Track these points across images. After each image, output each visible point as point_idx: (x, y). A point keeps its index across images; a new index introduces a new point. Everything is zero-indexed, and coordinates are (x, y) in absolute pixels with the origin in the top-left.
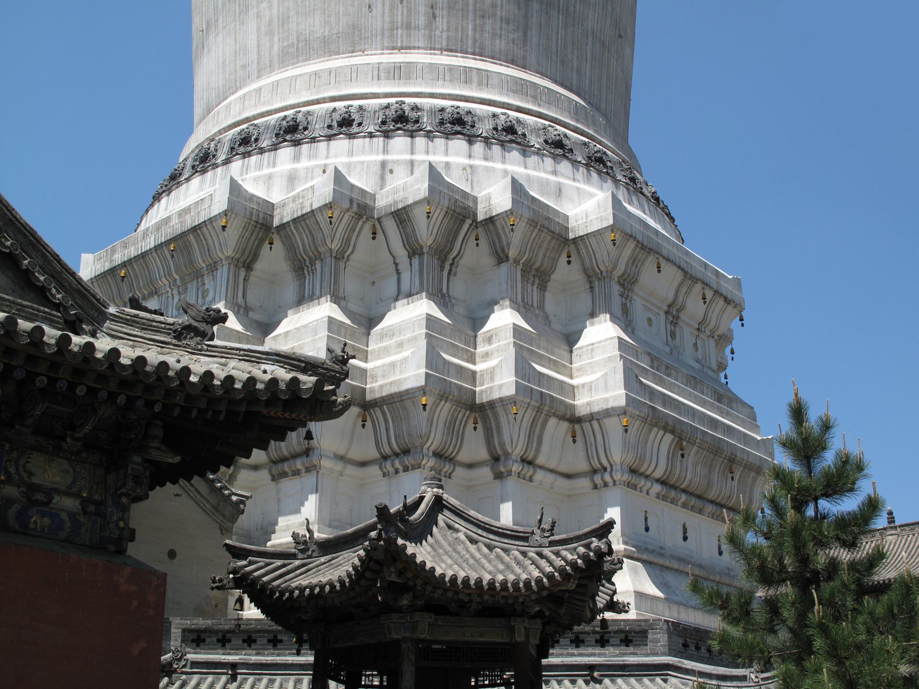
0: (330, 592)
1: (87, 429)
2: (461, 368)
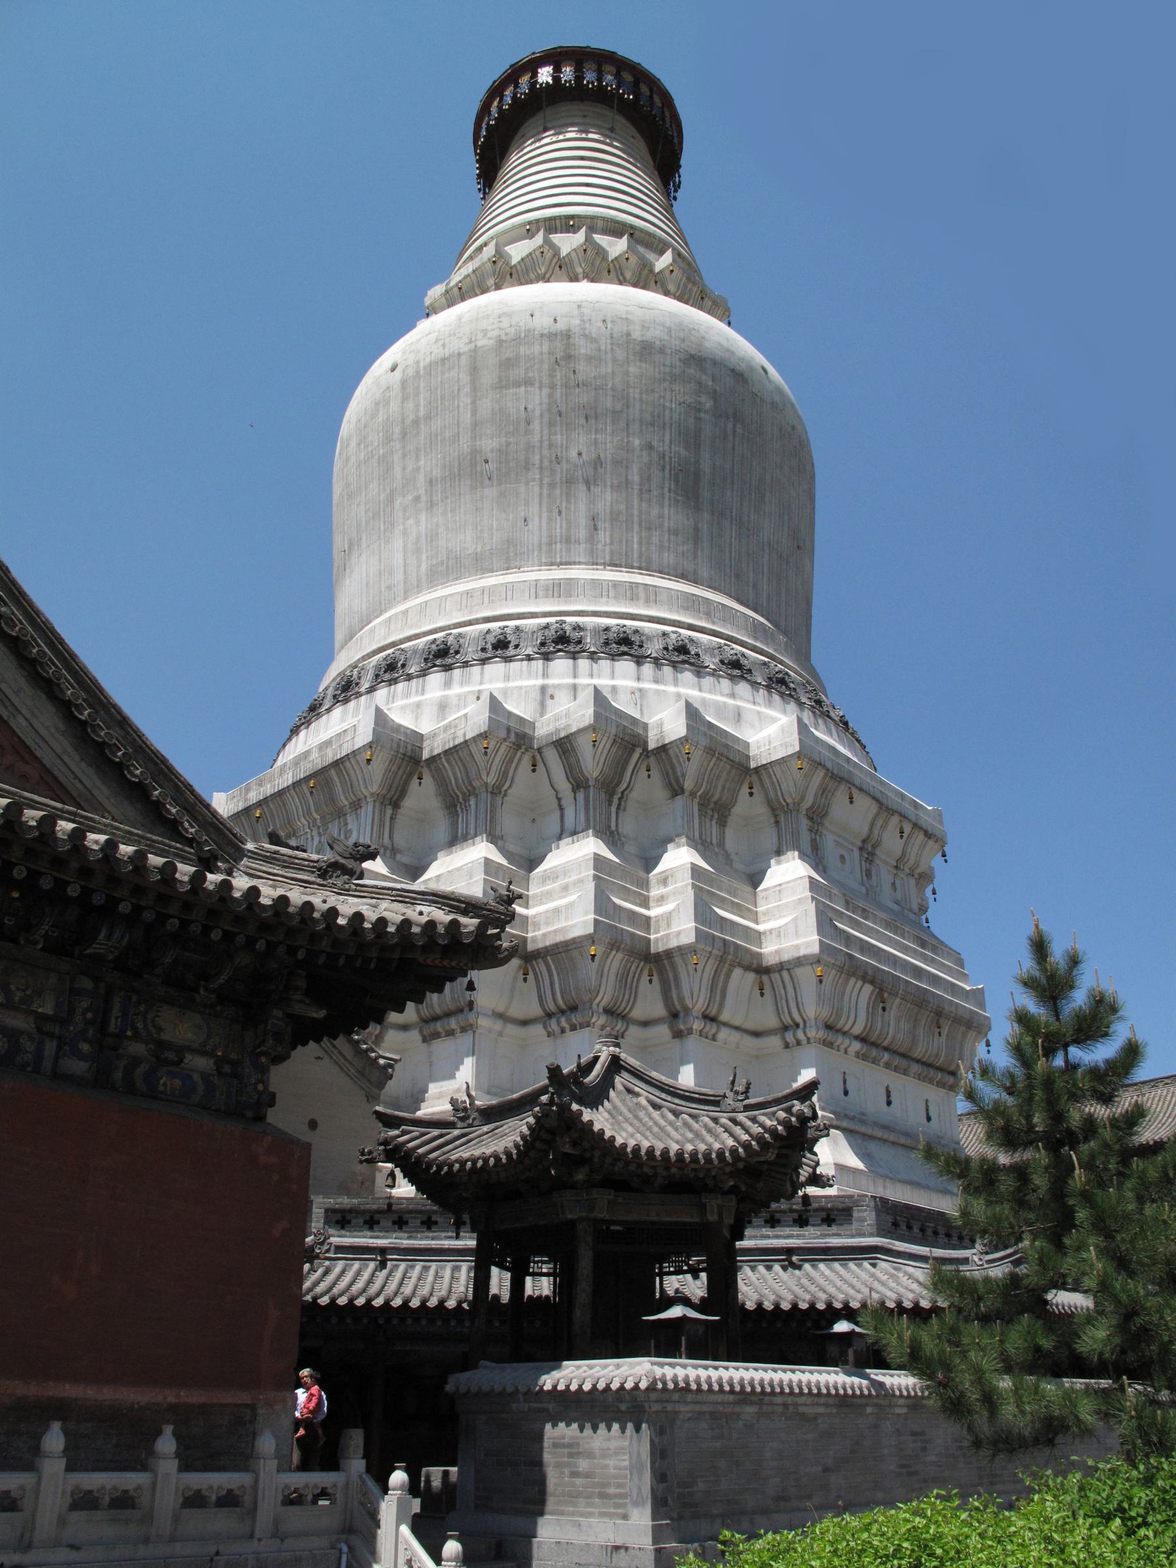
0: (495, 1165)
1: (223, 979)
2: (633, 913)
